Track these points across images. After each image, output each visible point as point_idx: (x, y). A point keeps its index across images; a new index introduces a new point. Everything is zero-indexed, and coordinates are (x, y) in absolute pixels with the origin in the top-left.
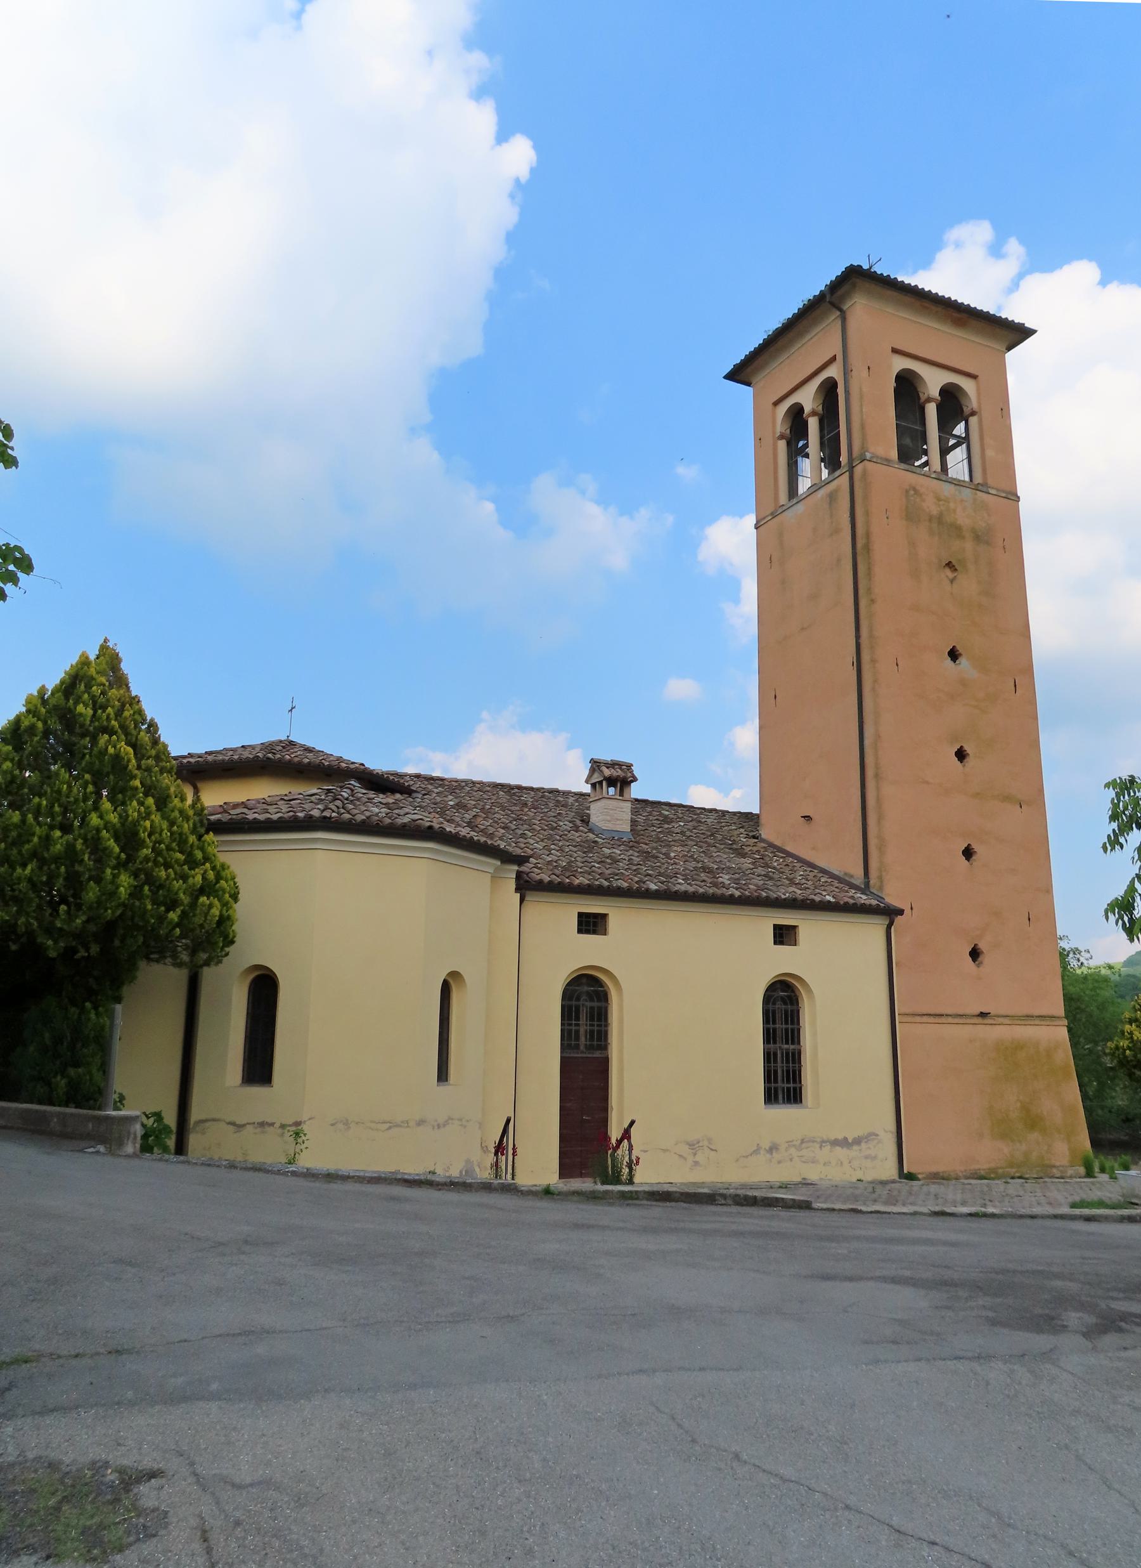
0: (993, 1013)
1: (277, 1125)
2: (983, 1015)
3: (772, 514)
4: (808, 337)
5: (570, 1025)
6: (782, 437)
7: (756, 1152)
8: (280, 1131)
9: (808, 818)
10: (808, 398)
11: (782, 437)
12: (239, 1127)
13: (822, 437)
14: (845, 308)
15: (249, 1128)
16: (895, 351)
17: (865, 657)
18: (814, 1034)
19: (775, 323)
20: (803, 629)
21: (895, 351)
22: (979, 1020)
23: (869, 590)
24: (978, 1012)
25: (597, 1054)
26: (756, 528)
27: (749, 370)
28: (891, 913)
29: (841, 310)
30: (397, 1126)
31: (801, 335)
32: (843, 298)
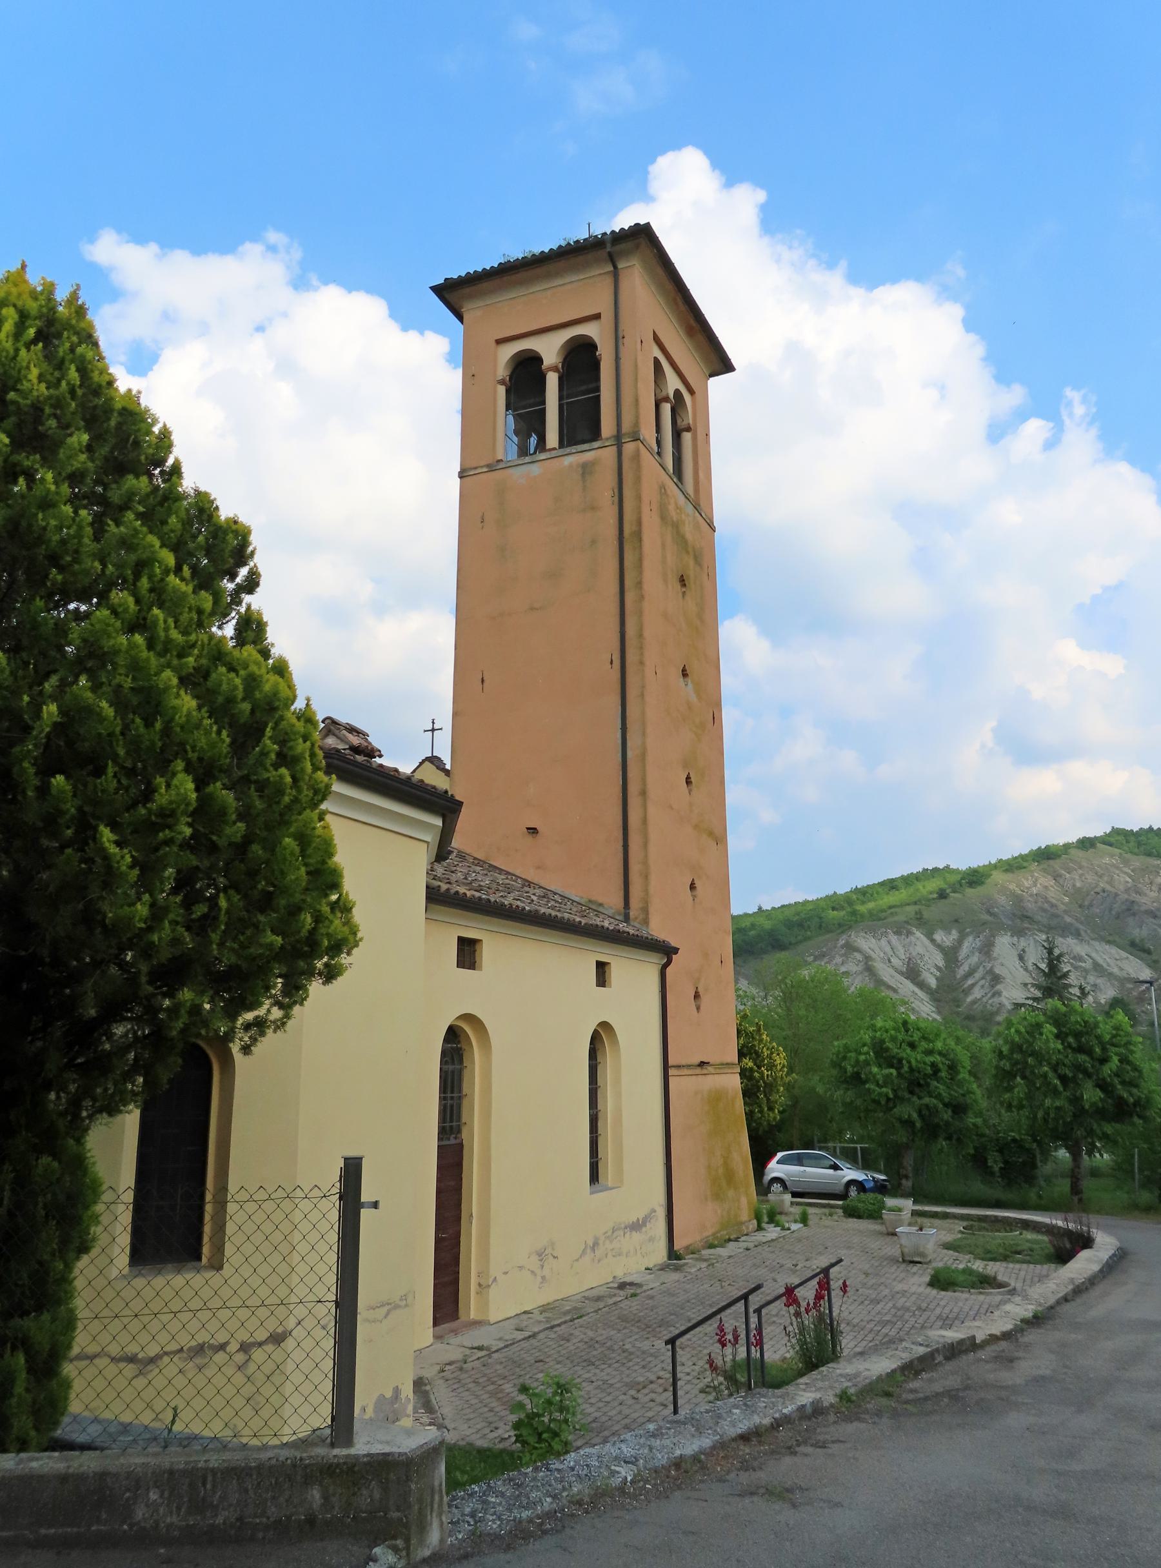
0: (712, 1062)
1: (233, 1347)
2: (702, 1064)
3: (488, 466)
4: (559, 281)
5: (452, 1098)
6: (502, 382)
7: (584, 1252)
8: (240, 1358)
9: (533, 831)
10: (550, 350)
11: (502, 382)
12: (144, 1364)
13: (561, 398)
14: (620, 266)
15: (170, 1367)
16: (499, 342)
17: (631, 657)
18: (618, 1095)
19: (516, 253)
20: (532, 609)
21: (499, 342)
22: (698, 1071)
23: (639, 584)
24: (697, 1061)
25: (452, 1141)
26: (461, 477)
27: (466, 291)
28: (668, 952)
29: (615, 267)
30: (397, 1307)
31: (549, 276)
32: (626, 254)
